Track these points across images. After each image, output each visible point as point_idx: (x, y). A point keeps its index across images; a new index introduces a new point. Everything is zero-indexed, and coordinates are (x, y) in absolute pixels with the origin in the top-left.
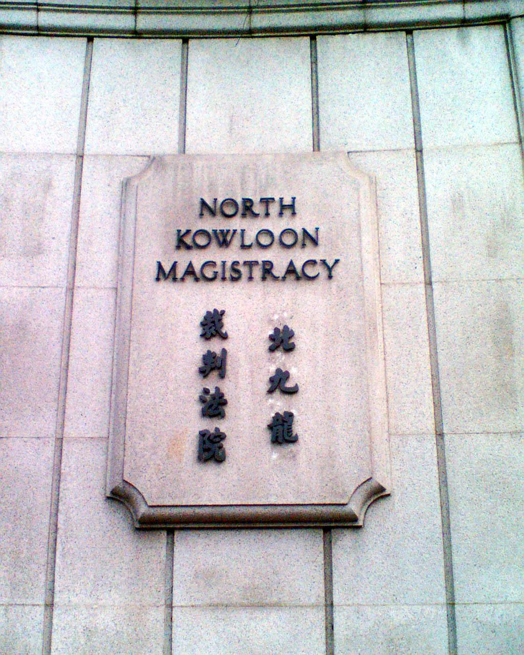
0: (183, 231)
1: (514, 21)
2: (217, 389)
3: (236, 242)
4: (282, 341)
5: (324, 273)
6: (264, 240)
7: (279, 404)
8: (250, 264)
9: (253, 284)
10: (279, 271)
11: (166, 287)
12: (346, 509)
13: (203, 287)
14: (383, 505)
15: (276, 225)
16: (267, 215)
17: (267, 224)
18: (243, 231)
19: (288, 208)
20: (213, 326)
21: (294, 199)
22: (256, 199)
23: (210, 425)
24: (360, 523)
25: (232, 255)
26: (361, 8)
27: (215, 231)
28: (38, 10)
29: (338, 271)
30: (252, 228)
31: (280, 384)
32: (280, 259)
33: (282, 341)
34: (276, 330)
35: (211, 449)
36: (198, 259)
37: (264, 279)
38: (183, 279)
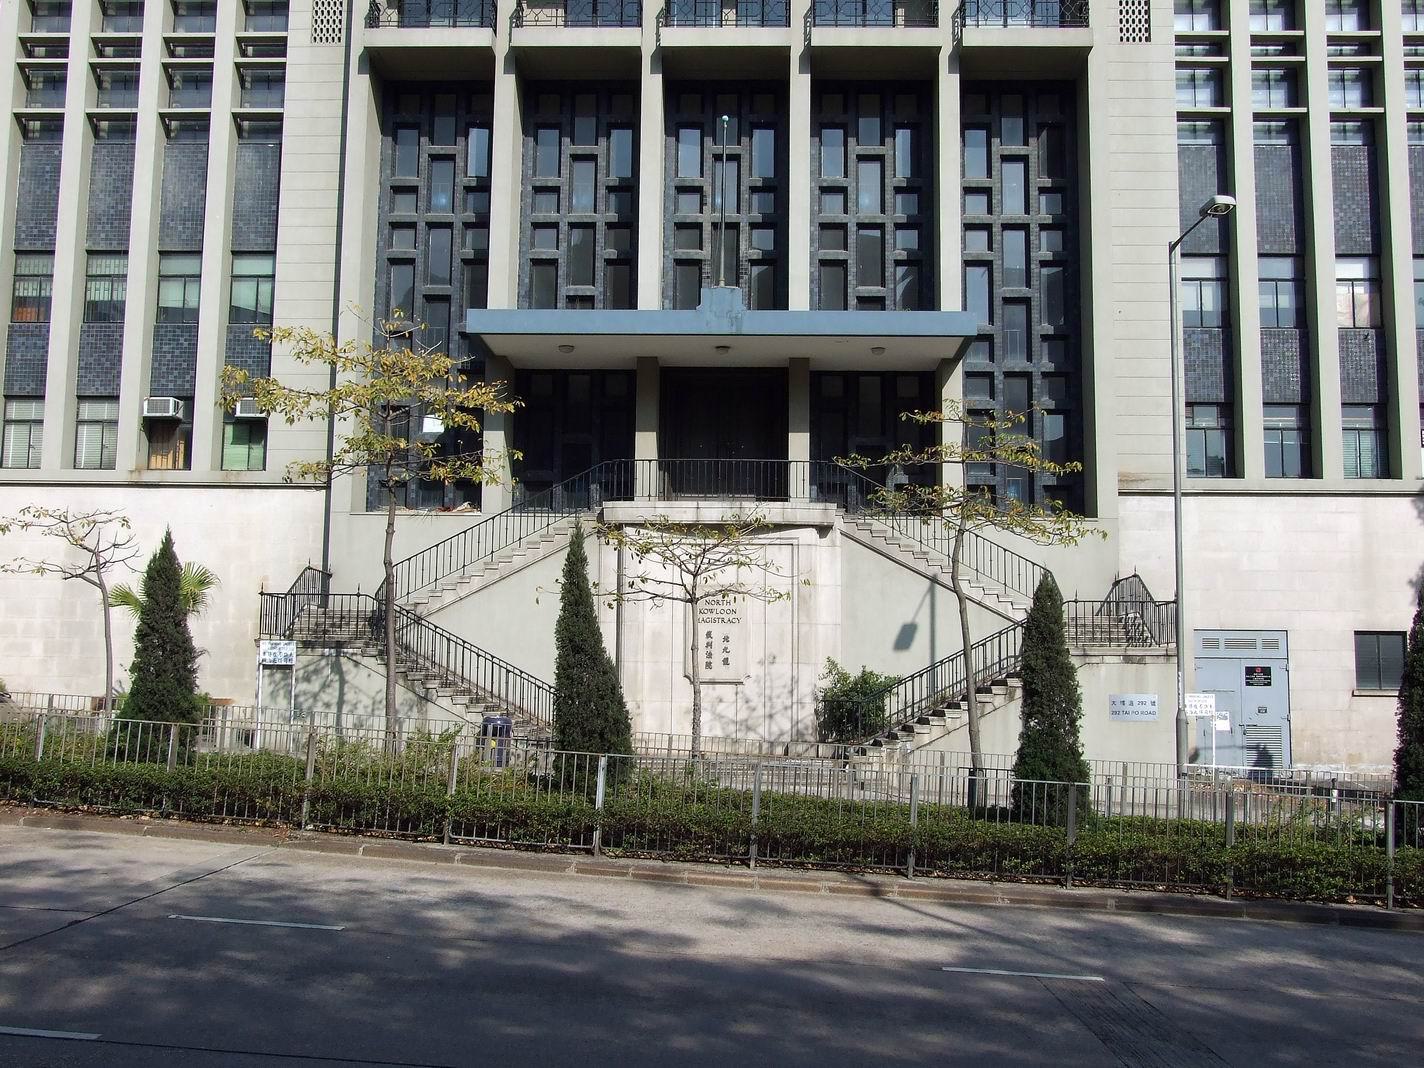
4: (726, 639)
7: (725, 655)
23: (708, 660)
25: (714, 615)
30: (719, 608)
31: (725, 649)
32: (726, 617)
33: (726, 639)
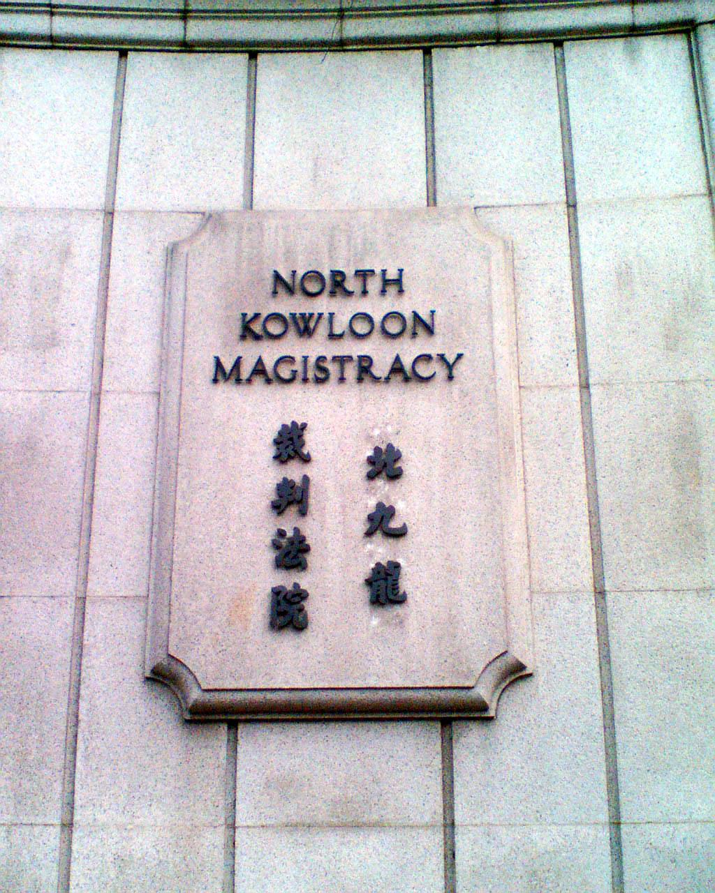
0: (250, 315)
1: (701, 28)
2: (296, 530)
3: (322, 330)
4: (385, 465)
5: (441, 372)
6: (361, 327)
8: (342, 360)
9: (345, 387)
10: (381, 369)
11: (226, 391)
12: (472, 694)
13: (277, 391)
14: (523, 688)
15: (377, 307)
16: (365, 293)
17: (364, 306)
18: (332, 315)
19: (394, 284)
20: (290, 444)
21: (401, 271)
22: (349, 272)
24: (492, 713)
26: (492, 11)
27: (293, 315)
28: (52, 14)
29: (461, 370)
33: (385, 465)
34: (377, 450)
35: (288, 612)
36: (270, 353)
37: (360, 380)
38: (249, 381)
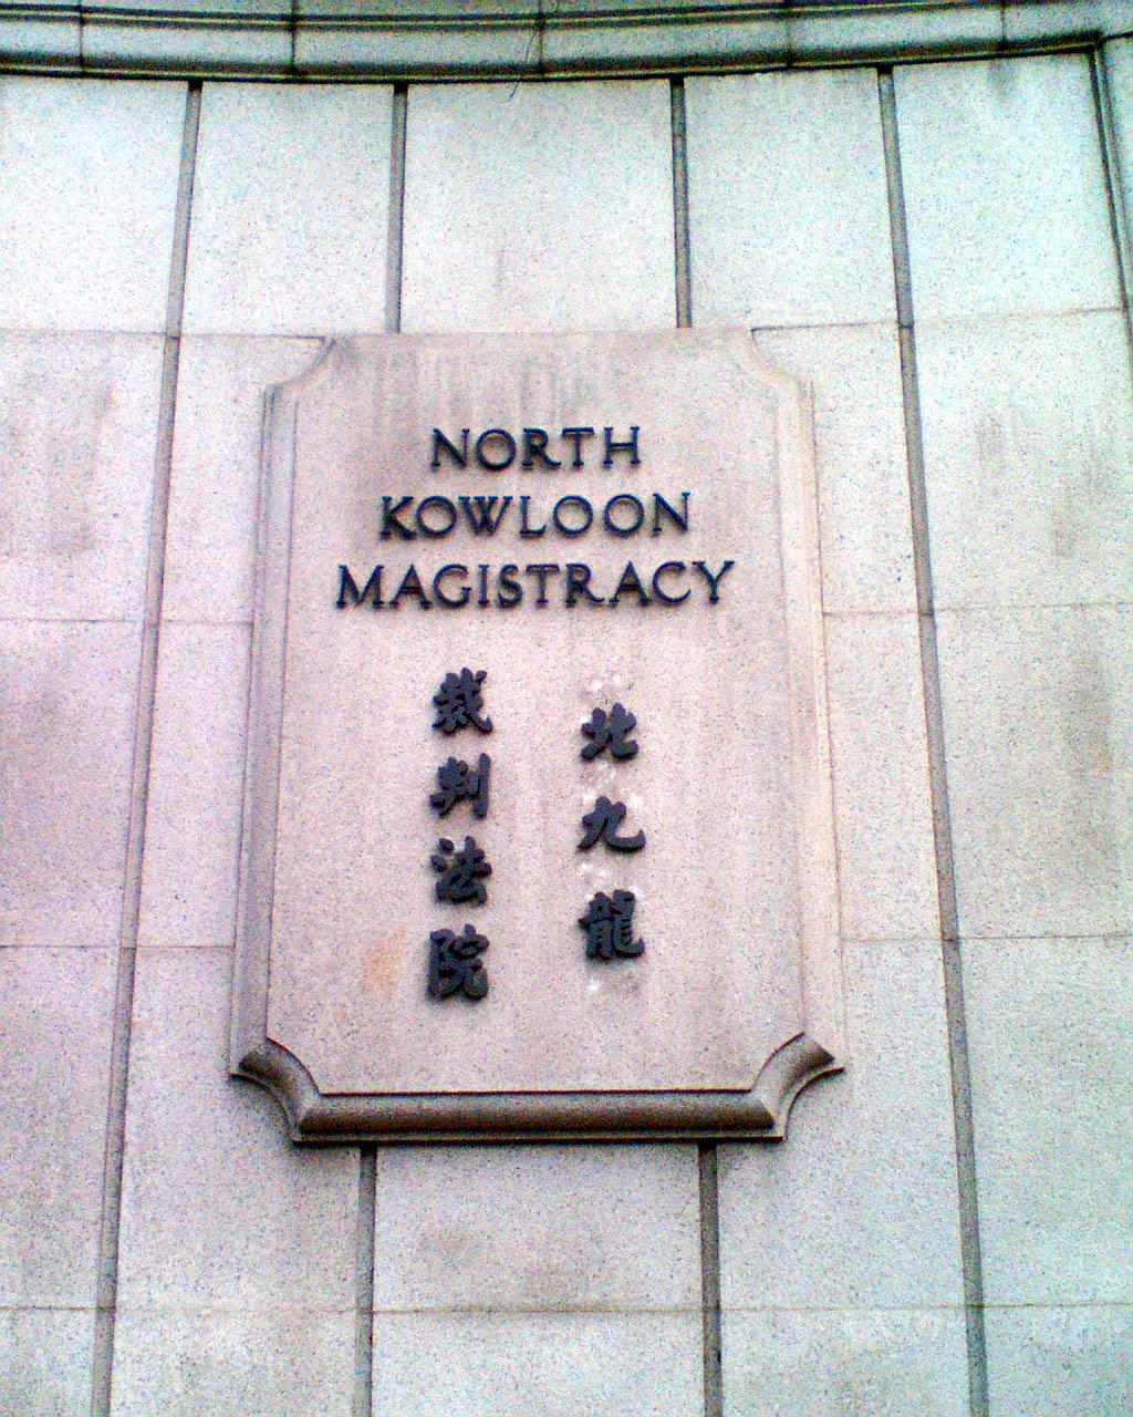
0: (396, 500)
1: (1111, 45)
2: (470, 841)
3: (511, 524)
4: (609, 738)
5: (700, 591)
6: (572, 520)
8: (542, 572)
9: (547, 613)
10: (604, 585)
11: (358, 620)
12: (748, 1101)
13: (438, 620)
14: (829, 1092)
15: (597, 487)
16: (578, 464)
17: (577, 485)
18: (525, 499)
19: (624, 451)
20: (459, 705)
21: (635, 430)
22: (554, 431)
24: (779, 1132)
26: (779, 17)
27: (465, 500)
28: (83, 22)
29: (730, 587)
33: (609, 738)
34: (598, 714)
35: (456, 971)
36: (428, 560)
37: (570, 603)
38: (395, 604)
